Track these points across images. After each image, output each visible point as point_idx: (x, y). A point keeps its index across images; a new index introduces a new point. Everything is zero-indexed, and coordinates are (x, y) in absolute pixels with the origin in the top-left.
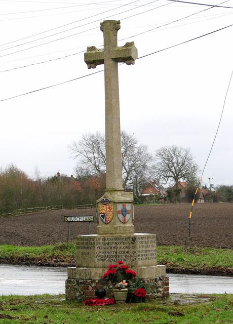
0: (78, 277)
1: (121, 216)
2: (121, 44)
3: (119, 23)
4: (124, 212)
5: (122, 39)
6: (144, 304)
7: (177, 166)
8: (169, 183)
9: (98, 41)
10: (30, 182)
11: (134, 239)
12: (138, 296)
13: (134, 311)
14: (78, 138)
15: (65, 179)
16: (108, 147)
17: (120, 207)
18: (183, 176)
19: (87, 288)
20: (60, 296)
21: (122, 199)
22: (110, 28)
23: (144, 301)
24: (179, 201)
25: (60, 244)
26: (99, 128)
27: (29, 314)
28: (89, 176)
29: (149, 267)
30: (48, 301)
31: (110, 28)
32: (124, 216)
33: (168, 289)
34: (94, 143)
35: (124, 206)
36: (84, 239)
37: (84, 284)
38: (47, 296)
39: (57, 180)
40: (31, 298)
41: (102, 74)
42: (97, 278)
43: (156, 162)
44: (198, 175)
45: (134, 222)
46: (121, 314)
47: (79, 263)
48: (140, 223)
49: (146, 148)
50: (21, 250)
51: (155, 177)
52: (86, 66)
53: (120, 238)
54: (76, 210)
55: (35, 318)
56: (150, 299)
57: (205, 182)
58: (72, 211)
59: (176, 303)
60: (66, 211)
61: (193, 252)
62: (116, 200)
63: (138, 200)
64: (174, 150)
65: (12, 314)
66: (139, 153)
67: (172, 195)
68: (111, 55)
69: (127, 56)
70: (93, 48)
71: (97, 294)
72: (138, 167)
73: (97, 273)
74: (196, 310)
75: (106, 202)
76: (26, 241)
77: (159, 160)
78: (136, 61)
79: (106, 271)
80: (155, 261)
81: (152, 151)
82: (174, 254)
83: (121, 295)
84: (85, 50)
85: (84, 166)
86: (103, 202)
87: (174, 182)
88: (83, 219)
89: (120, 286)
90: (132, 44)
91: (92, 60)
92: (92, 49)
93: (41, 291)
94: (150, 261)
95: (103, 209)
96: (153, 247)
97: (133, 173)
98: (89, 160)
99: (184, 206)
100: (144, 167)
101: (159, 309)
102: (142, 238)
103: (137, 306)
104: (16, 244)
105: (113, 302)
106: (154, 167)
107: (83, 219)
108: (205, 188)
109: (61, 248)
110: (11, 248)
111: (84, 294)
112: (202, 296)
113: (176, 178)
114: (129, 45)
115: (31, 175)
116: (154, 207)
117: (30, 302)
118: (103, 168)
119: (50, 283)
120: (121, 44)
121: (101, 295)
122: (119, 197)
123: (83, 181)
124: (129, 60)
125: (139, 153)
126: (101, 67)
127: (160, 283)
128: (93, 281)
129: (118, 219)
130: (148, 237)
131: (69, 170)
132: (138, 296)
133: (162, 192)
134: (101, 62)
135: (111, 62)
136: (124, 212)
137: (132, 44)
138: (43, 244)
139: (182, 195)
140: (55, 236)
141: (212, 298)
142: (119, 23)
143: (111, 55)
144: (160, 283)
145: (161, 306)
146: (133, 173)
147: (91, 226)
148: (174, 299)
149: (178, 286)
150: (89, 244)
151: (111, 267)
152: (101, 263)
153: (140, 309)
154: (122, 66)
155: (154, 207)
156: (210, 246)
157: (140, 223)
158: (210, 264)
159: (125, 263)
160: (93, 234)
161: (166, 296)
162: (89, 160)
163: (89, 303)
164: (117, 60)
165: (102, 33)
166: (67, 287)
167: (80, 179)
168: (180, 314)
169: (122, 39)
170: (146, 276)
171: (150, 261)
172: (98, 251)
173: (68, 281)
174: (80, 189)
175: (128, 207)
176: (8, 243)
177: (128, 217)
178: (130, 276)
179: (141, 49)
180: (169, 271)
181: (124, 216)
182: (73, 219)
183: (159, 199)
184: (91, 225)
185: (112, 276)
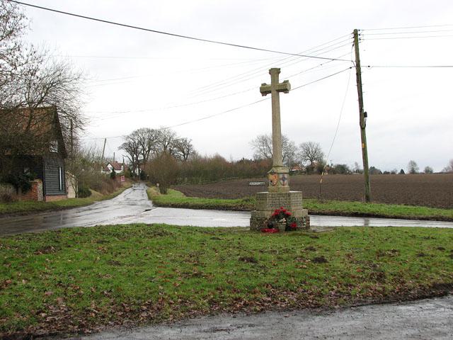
0: (257, 216)
1: (282, 181)
2: (281, 81)
3: (280, 69)
4: (283, 179)
5: (281, 79)
6: (295, 232)
7: (312, 153)
8: (307, 163)
9: (268, 81)
10: (227, 163)
11: (289, 195)
12: (292, 227)
13: (290, 236)
14: (255, 138)
15: (247, 161)
16: (274, 143)
17: (281, 176)
18: (315, 159)
19: (263, 223)
20: (247, 227)
21: (283, 171)
22: (275, 72)
23: (295, 230)
24: (313, 173)
25: (246, 198)
26: (268, 131)
27: (230, 237)
28: (261, 160)
29: (298, 211)
30: (240, 230)
31: (275, 72)
32: (284, 181)
33: (309, 223)
34: (264, 141)
35: (283, 176)
36: (262, 194)
37: (261, 220)
38: (240, 227)
39: (243, 162)
40: (230, 228)
41: (270, 100)
42: (268, 217)
43: (300, 151)
44: (324, 159)
45: (289, 185)
46: (282, 237)
47: (257, 208)
48: (293, 185)
49: (294, 143)
50: (223, 202)
51: (299, 160)
52: (261, 94)
53: (281, 194)
54: (254, 179)
55: (233, 239)
56: (299, 229)
57: (329, 163)
58: (251, 180)
59: (314, 231)
60: (248, 180)
61: (322, 202)
62: (279, 172)
63: (291, 173)
64: (310, 144)
65: (220, 237)
66: (290, 146)
67: (309, 170)
68: (275, 88)
69: (285, 88)
70: (265, 84)
71: (268, 226)
72: (290, 154)
73: (268, 214)
74: (326, 235)
75: (273, 173)
76: (225, 197)
77: (302, 150)
78: (290, 92)
79: (273, 213)
80: (301, 207)
81: (297, 145)
82: (312, 203)
83: (282, 227)
84: (260, 86)
85: (258, 154)
86: (271, 173)
87: (310, 163)
88: (259, 183)
89: (279, 222)
90: (287, 81)
91: (264, 91)
92: (264, 84)
93: (236, 225)
94: (299, 207)
95: (271, 177)
96: (300, 199)
97: (287, 157)
98: (261, 150)
99: (316, 176)
100: (293, 154)
101: (304, 235)
102: (294, 194)
103: (291, 233)
104: (220, 198)
105: (278, 231)
106: (298, 154)
107: (259, 183)
108: (328, 166)
109: (246, 201)
110: (218, 200)
111: (262, 226)
112: (329, 227)
113: (311, 161)
114: (286, 82)
115: (228, 159)
116: (300, 177)
117: (230, 230)
118: (269, 155)
119: (241, 221)
120: (281, 81)
121: (270, 227)
122: (280, 170)
123: (258, 162)
124: (286, 91)
125: (290, 146)
126: (269, 95)
127: (304, 220)
128: (266, 219)
129: (280, 183)
130: (298, 193)
131: (250, 156)
132: (292, 227)
133: (304, 169)
134: (270, 92)
135: (275, 92)
136: (283, 179)
137: (287, 81)
138: (236, 198)
139: (315, 170)
140: (242, 194)
141: (335, 228)
142: (280, 69)
143: (275, 88)
144: (304, 220)
145: (306, 233)
146: (287, 157)
147: (265, 187)
148: (313, 229)
149: (315, 222)
150: (263, 197)
151: (276, 211)
152: (270, 208)
153: (293, 235)
154: (281, 94)
155: (300, 177)
156: (332, 199)
157: (293, 185)
158: (333, 209)
159: (284, 209)
160: (221, 231)
161: (308, 227)
162: (261, 150)
163: (264, 231)
164: (279, 91)
165: (270, 76)
166: (251, 222)
167: (256, 161)
168: (316, 238)
169: (281, 79)
170: (297, 216)
171: (299, 207)
172: (269, 201)
173: (252, 219)
174: (255, 167)
175: (286, 176)
176: (216, 198)
177: (286, 181)
178: (287, 216)
179: (293, 83)
180: (309, 213)
181: (284, 181)
182: (253, 184)
183: (301, 172)
184: (263, 187)
185: (277, 216)
